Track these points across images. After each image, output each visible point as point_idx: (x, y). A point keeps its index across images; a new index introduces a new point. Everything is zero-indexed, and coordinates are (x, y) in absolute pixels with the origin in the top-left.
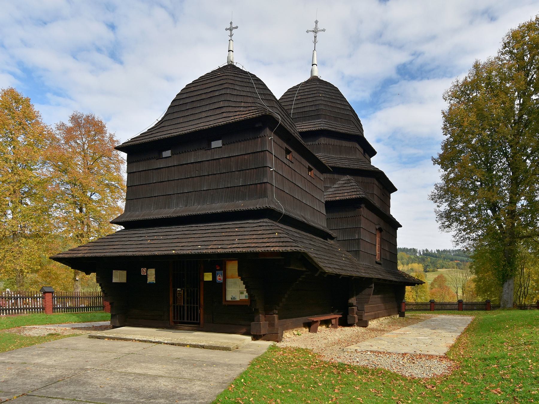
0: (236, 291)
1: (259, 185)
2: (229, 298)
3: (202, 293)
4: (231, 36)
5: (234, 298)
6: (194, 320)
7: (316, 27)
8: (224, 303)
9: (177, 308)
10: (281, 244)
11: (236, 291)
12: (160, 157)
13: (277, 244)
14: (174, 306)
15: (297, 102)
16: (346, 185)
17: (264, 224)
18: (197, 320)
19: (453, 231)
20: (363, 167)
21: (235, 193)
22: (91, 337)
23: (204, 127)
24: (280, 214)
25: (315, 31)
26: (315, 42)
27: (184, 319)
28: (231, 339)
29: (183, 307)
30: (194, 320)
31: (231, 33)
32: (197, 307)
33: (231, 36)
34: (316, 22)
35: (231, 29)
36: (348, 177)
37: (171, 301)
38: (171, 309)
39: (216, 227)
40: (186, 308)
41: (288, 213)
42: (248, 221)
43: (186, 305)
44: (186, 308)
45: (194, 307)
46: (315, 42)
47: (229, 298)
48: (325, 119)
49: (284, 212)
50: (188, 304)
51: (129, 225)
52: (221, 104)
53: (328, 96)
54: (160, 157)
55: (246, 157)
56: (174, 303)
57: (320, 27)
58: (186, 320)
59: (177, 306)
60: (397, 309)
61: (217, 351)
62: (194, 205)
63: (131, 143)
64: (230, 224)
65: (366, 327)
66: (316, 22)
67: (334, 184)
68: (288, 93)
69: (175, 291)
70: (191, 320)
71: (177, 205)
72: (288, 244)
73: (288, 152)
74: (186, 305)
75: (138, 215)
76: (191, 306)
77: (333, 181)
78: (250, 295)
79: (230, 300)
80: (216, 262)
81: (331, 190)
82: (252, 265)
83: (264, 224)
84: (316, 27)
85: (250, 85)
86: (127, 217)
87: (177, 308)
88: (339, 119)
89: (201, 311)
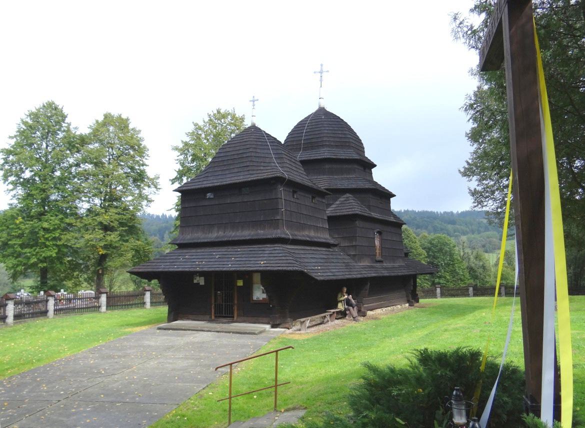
0: (259, 294)
2: (255, 298)
4: (254, 105)
7: (322, 70)
8: (251, 302)
10: (287, 265)
11: (259, 294)
12: (205, 198)
13: (285, 265)
14: (215, 305)
15: (307, 134)
16: (345, 202)
17: (278, 248)
20: (362, 185)
21: (256, 224)
22: (159, 329)
24: (289, 239)
25: (321, 72)
26: (321, 81)
27: (222, 314)
29: (222, 305)
30: (230, 314)
31: (254, 103)
33: (254, 105)
34: (322, 65)
35: (254, 101)
36: (348, 195)
38: (213, 306)
39: (246, 250)
40: (224, 306)
41: (295, 238)
43: (224, 304)
44: (224, 306)
46: (321, 81)
47: (255, 298)
49: (291, 237)
50: (225, 302)
51: (182, 246)
52: (248, 164)
53: (331, 129)
54: (205, 198)
55: (265, 202)
56: (215, 302)
57: (324, 69)
60: (406, 298)
61: (225, 364)
64: (256, 247)
65: (364, 316)
66: (322, 65)
67: (336, 201)
68: (300, 126)
69: (216, 294)
73: (294, 192)
74: (224, 304)
78: (269, 296)
80: (247, 275)
81: (334, 206)
82: (271, 279)
83: (278, 248)
84: (322, 70)
86: (181, 240)
89: (235, 308)
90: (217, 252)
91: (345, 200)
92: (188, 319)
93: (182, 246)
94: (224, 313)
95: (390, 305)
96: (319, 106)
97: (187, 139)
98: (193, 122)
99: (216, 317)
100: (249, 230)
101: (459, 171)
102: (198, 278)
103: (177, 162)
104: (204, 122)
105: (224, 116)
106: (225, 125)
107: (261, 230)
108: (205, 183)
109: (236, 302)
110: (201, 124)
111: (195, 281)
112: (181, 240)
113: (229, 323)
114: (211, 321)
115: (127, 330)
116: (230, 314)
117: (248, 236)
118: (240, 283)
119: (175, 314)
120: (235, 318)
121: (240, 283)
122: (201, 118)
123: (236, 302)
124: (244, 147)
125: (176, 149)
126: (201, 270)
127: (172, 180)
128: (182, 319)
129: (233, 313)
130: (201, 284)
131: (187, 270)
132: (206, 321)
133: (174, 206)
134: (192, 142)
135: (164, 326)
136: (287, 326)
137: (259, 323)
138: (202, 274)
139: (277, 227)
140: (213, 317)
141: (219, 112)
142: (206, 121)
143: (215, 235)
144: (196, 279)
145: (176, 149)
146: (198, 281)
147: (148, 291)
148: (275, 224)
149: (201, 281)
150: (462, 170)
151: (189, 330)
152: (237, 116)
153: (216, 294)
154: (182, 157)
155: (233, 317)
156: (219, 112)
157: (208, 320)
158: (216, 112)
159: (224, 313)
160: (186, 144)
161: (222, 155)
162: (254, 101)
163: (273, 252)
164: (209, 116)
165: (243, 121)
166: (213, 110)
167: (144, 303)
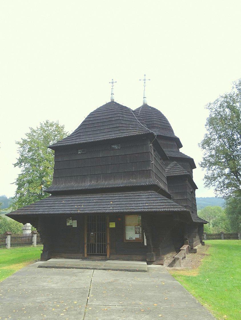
1: (146, 171)
2: (128, 238)
3: (108, 234)
5: (132, 238)
6: (102, 253)
9: (90, 246)
11: (131, 234)
14: (88, 245)
18: (105, 253)
19: (212, 188)
22: (40, 267)
23: (110, 138)
27: (95, 252)
28: (134, 264)
29: (95, 244)
32: (105, 244)
35: (112, 83)
37: (86, 241)
38: (86, 245)
40: (96, 245)
42: (141, 192)
43: (97, 244)
44: (96, 245)
45: (103, 244)
47: (128, 238)
48: (158, 129)
51: (55, 194)
57: (147, 78)
58: (96, 253)
59: (90, 244)
62: (102, 181)
63: (57, 145)
64: (130, 194)
67: (167, 166)
69: (89, 235)
70: (100, 253)
71: (91, 181)
72: (175, 207)
74: (97, 244)
75: (62, 186)
76: (103, 244)
77: (167, 165)
79: (129, 239)
80: (120, 218)
85: (131, 115)
86: (56, 188)
87: (90, 246)
88: (164, 129)
89: (108, 247)
90: (95, 198)
91: (174, 166)
92: (61, 257)
93: (55, 194)
94: (96, 251)
95: (198, 244)
96: (144, 103)
97: (26, 138)
98: (29, 128)
99: (88, 255)
100: (121, 179)
101: (199, 163)
102: (71, 221)
103: (18, 152)
104: (37, 128)
105: (52, 125)
106: (51, 131)
107: (133, 179)
108: (78, 140)
109: (108, 242)
110: (35, 129)
111: (68, 224)
112: (56, 188)
113: (102, 260)
114: (83, 258)
115: (5, 268)
116: (90, 252)
117: (122, 184)
118: (113, 225)
119: (46, 255)
120: (108, 256)
121: (113, 225)
122: (36, 126)
123: (108, 242)
124: (113, 113)
125: (18, 143)
126: (82, 212)
127: (15, 164)
128: (55, 257)
129: (105, 252)
130: (73, 226)
131: (68, 212)
132: (79, 258)
133: (16, 181)
134: (29, 140)
135: (44, 264)
136: (161, 263)
137: (133, 260)
138: (74, 216)
139: (150, 177)
140: (86, 255)
141: (47, 122)
142: (38, 128)
143: (87, 184)
144: (69, 222)
145: (18, 143)
146: (70, 224)
147: (9, 235)
148: (147, 173)
149: (74, 224)
150: (200, 163)
151: (73, 268)
152: (59, 126)
153: (89, 235)
154: (21, 149)
155: (106, 255)
156: (47, 122)
157: (82, 258)
158: (46, 122)
159: (96, 251)
160: (25, 141)
161: (92, 119)
162: (112, 83)
163: (149, 196)
164: (41, 124)
165: (63, 129)
166: (44, 121)
167: (6, 244)
